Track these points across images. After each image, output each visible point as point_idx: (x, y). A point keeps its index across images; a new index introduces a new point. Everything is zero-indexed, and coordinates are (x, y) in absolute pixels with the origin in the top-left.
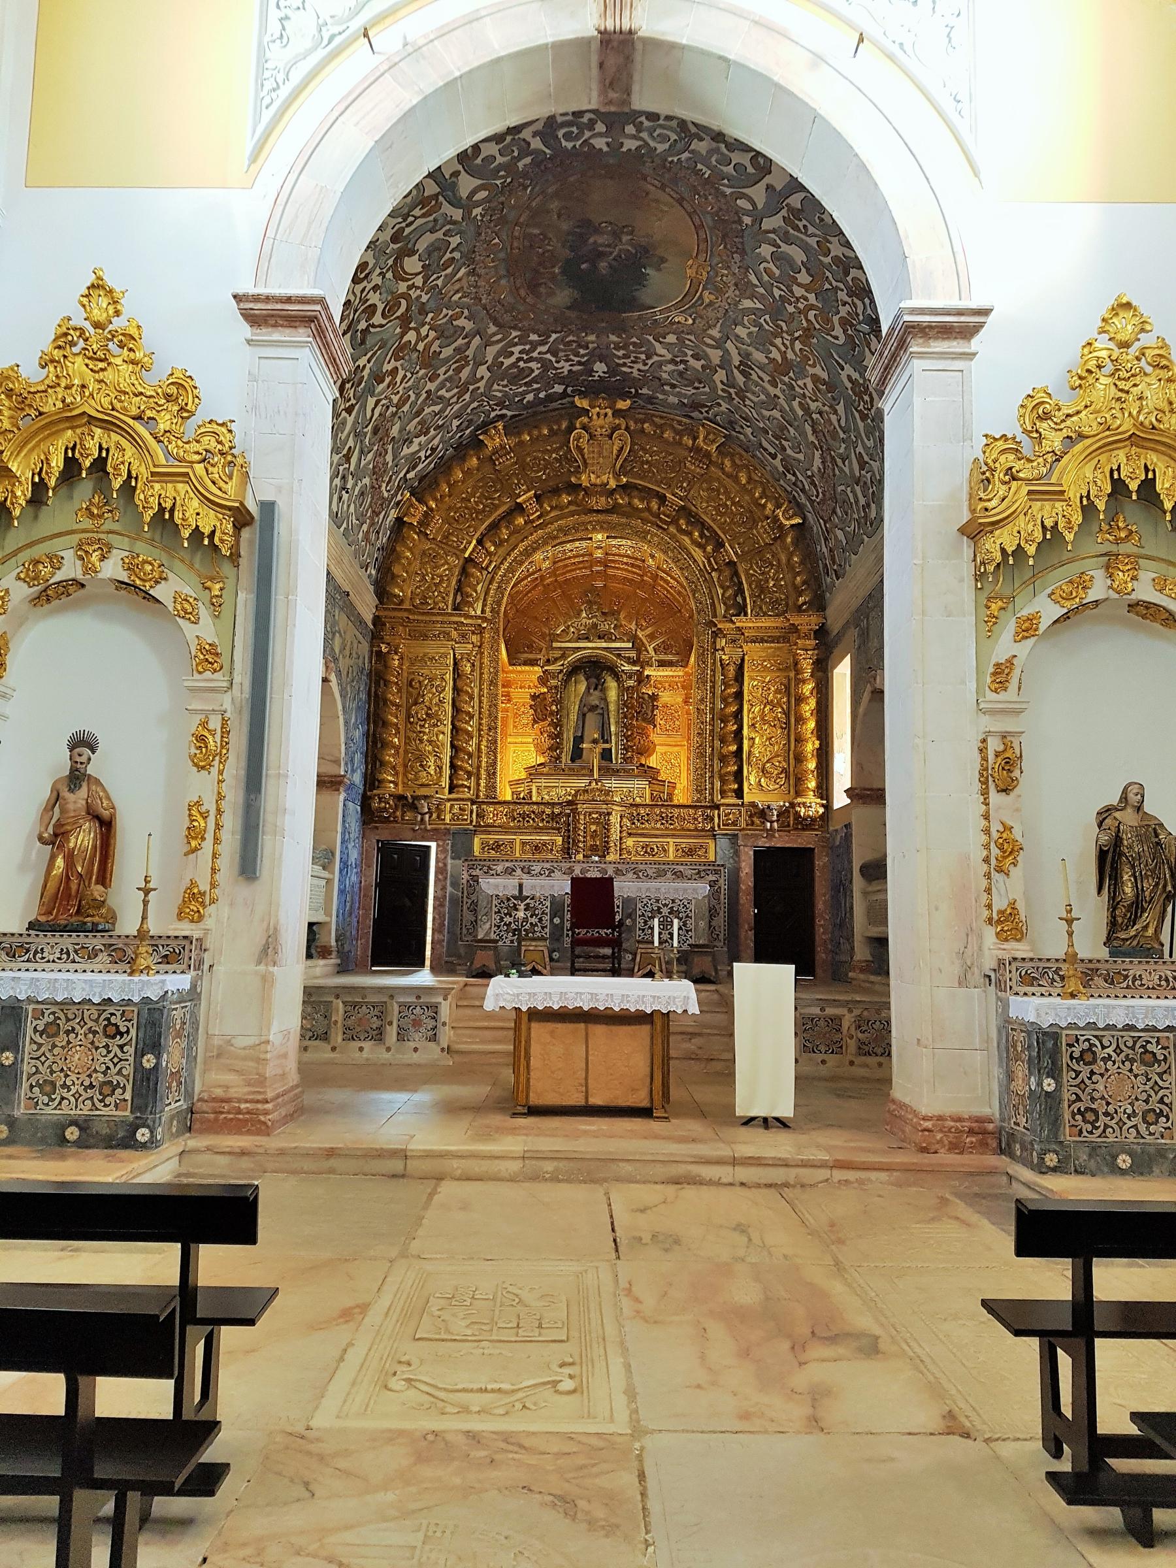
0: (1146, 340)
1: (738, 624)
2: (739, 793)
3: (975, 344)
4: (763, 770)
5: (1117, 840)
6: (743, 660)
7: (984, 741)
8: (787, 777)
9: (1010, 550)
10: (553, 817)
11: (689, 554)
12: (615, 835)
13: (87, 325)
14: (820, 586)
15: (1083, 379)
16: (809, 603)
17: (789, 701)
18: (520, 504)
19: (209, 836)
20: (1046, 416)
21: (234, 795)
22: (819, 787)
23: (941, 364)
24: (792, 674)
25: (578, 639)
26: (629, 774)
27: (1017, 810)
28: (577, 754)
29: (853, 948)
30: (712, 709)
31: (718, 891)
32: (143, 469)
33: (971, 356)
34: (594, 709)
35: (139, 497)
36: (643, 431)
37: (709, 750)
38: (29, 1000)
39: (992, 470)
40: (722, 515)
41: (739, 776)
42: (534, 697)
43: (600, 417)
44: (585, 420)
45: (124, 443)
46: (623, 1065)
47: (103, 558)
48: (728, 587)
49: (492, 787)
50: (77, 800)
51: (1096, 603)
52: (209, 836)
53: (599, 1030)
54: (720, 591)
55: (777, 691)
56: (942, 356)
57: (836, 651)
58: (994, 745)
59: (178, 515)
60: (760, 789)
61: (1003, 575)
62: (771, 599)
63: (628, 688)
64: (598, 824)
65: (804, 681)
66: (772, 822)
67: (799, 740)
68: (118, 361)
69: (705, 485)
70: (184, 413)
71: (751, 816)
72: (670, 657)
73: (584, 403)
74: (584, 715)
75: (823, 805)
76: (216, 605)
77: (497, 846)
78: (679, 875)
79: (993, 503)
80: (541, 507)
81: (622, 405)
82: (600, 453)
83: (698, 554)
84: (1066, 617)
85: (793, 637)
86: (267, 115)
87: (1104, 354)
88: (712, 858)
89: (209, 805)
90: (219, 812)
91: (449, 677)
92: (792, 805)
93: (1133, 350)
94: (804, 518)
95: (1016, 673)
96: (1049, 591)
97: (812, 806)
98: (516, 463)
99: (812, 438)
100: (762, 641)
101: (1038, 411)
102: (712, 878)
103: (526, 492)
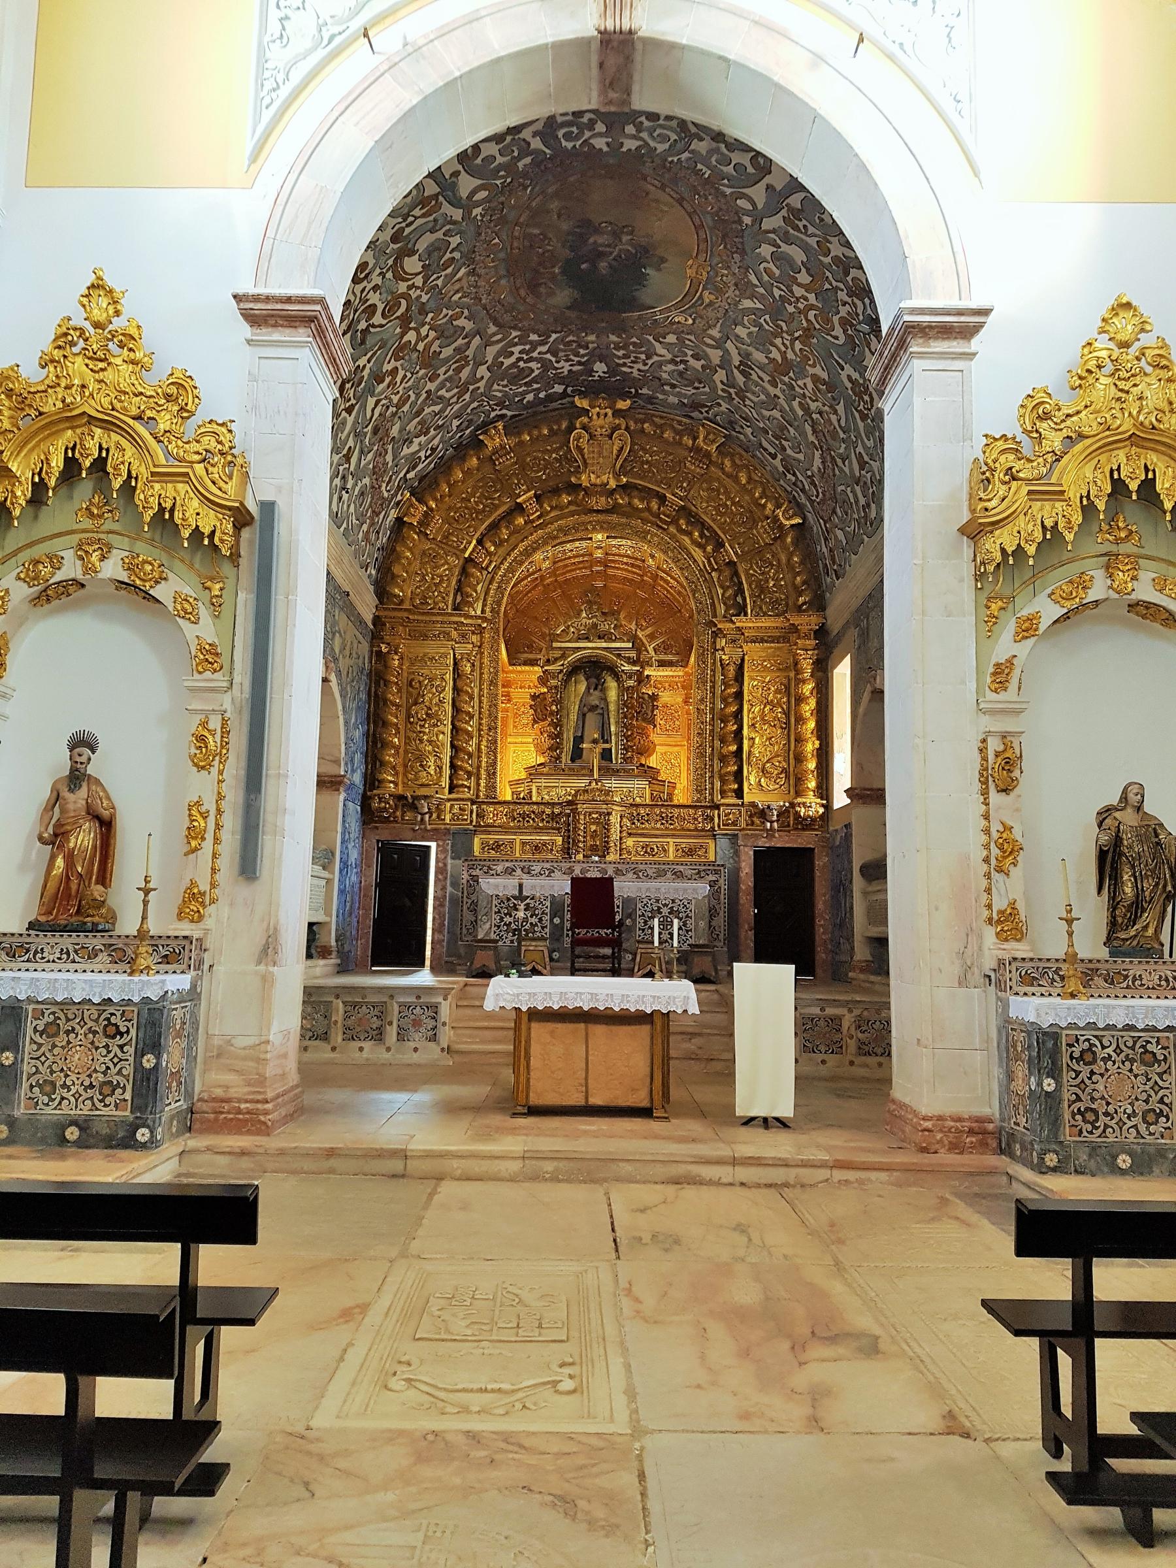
0: (1146, 340)
1: (738, 624)
2: (739, 793)
3: (975, 344)
4: (763, 770)
5: (1117, 840)
6: (743, 660)
7: (984, 741)
8: (787, 777)
9: (1010, 550)
10: (553, 817)
11: (689, 554)
12: (615, 835)
13: (87, 325)
14: (820, 586)
15: (1083, 379)
16: (809, 603)
17: (789, 701)
18: (520, 504)
19: (209, 836)
20: (1046, 416)
21: (234, 795)
22: (819, 787)
23: (941, 364)
24: (792, 674)
25: (578, 639)
26: (629, 774)
27: (1017, 810)
28: (577, 754)
29: (853, 948)
30: (712, 709)
31: (718, 891)
32: (143, 469)
33: (971, 356)
34: (594, 709)
35: (139, 497)
36: (643, 431)
37: (709, 750)
38: (29, 1000)
39: (992, 470)
40: (722, 515)
41: (739, 776)
42: (534, 697)
43: (600, 417)
44: (585, 420)
45: (124, 443)
46: (623, 1065)
47: (103, 558)
48: (728, 587)
49: (492, 787)
50: (77, 800)
51: (1096, 603)
52: (209, 836)
53: (599, 1030)
54: (720, 591)
55: (777, 691)
56: (942, 356)
57: (836, 651)
58: (994, 745)
59: (178, 515)
60: (760, 789)
61: (1003, 575)
62: (771, 599)
63: (628, 688)
64: (598, 824)
65: (804, 681)
66: (772, 822)
67: (799, 740)
68: (118, 361)
69: (705, 485)
70: (184, 413)
71: (751, 816)
72: (670, 657)
73: (584, 403)
74: (584, 715)
75: (823, 805)
76: (216, 605)
77: (497, 846)
78: (679, 875)
79: (993, 503)
80: (541, 507)
81: (622, 405)
82: (600, 453)
83: (698, 554)
84: (1066, 617)
85: (793, 637)
86: (267, 115)
87: (1104, 354)
88: (712, 858)
89: (209, 805)
90: (219, 812)
91: (449, 677)
92: (792, 805)
93: (1133, 350)
94: (804, 518)
95: (1016, 673)
96: (1049, 591)
97: (812, 806)
98: (516, 463)
99: (812, 438)
100: (762, 641)
101: (1038, 411)
102: (712, 878)
103: (526, 492)
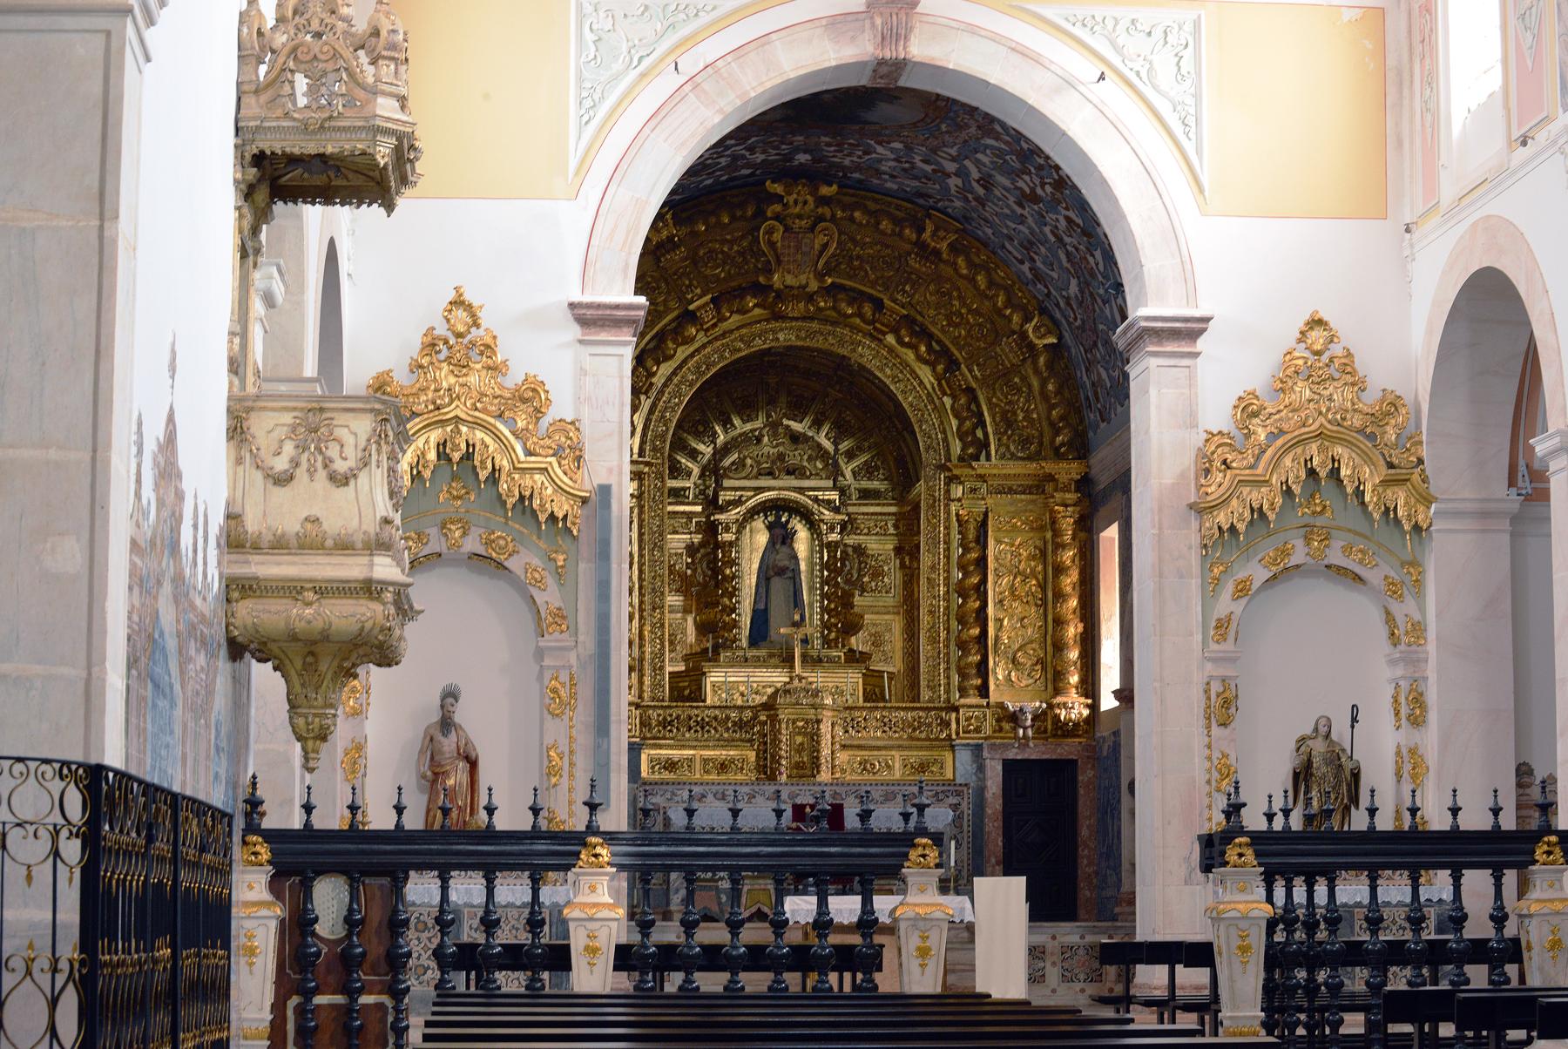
0: (1337, 350)
2: (983, 691)
3: (1201, 344)
5: (1309, 764)
6: (986, 514)
8: (1044, 669)
9: (1225, 527)
10: (740, 725)
11: (913, 372)
12: (825, 752)
13: (449, 334)
14: (1082, 420)
15: (1282, 386)
16: (1070, 444)
18: (693, 313)
19: (565, 774)
20: (1255, 415)
21: (584, 739)
22: (1083, 681)
23: (1172, 362)
24: (1049, 535)
25: (760, 474)
29: (1120, 880)
30: (947, 579)
32: (505, 463)
33: (1196, 355)
37: (943, 635)
38: (466, 905)
39: (1210, 461)
40: (957, 325)
41: (983, 669)
43: (799, 200)
44: (777, 208)
45: (488, 440)
47: (464, 534)
48: (966, 419)
52: (565, 774)
54: (955, 423)
55: (1032, 557)
57: (1103, 512)
58: (1216, 687)
59: (536, 503)
60: (1011, 686)
62: (1020, 436)
63: (829, 543)
64: (805, 734)
65: (1064, 546)
66: (1025, 728)
68: (478, 366)
70: (538, 413)
71: (999, 720)
72: (875, 484)
73: (778, 188)
74: (768, 579)
75: (1088, 706)
76: (559, 574)
77: (671, 765)
79: (1213, 488)
80: (719, 312)
81: (825, 190)
82: (798, 248)
83: (926, 374)
84: (1275, 577)
85: (1049, 488)
87: (1301, 362)
88: (949, 775)
90: (571, 752)
92: (1051, 706)
93: (1325, 358)
94: (1060, 338)
95: (1233, 626)
97: (1074, 707)
98: (686, 259)
99: (1066, 264)
100: (1011, 491)
101: (1248, 409)
103: (700, 297)
